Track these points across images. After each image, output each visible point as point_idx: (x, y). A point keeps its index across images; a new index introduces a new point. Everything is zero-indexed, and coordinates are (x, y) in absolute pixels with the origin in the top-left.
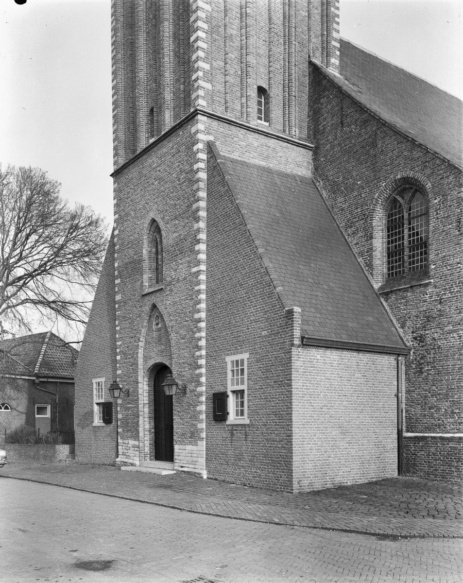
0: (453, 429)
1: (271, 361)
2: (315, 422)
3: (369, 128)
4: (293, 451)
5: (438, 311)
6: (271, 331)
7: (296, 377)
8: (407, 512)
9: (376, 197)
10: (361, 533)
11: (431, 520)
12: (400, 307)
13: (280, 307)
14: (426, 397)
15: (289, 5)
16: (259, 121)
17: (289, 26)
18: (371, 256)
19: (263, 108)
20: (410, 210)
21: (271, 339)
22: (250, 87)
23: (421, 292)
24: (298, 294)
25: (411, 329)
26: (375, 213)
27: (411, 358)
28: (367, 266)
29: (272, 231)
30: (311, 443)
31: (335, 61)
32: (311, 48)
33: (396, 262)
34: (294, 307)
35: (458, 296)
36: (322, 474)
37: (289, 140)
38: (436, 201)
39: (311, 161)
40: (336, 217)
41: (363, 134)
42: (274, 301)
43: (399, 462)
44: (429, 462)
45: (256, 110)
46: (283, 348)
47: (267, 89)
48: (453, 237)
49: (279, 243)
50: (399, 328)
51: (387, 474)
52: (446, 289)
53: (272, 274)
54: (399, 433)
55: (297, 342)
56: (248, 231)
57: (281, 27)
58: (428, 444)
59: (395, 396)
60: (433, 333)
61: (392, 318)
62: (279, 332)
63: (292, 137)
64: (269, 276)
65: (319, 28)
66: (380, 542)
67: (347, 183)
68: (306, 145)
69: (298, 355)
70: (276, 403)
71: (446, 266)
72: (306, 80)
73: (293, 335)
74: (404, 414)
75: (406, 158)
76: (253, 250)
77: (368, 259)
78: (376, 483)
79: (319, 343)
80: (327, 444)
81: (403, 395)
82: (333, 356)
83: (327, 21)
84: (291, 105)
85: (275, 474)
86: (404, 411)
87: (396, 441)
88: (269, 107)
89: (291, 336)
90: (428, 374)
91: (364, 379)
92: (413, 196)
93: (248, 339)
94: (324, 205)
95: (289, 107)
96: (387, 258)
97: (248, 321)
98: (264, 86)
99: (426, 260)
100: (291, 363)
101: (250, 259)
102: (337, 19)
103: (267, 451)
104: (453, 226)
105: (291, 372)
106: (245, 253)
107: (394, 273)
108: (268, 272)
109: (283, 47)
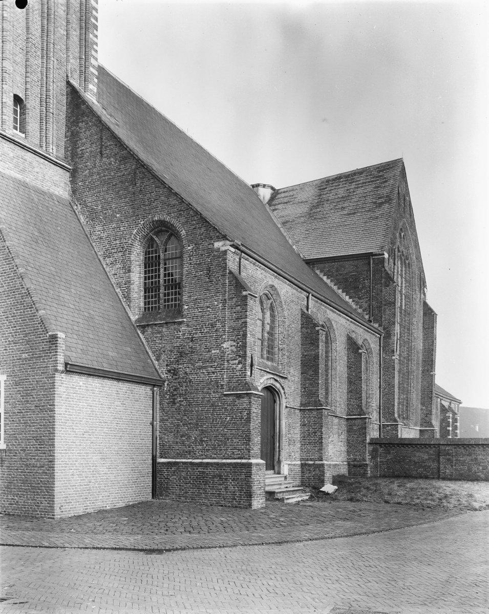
0: (202, 455)
1: (32, 384)
2: (76, 448)
3: (128, 165)
4: (56, 477)
5: (189, 348)
6: (33, 355)
7: (59, 402)
8: (167, 530)
9: (134, 233)
10: (130, 549)
11: (188, 535)
12: (155, 341)
13: (43, 331)
14: (178, 425)
15: (48, 20)
16: (15, 131)
17: (47, 40)
18: (128, 288)
19: (18, 117)
20: (166, 251)
21: (32, 362)
22: (6, 93)
23: (175, 329)
24: (59, 319)
25: (166, 363)
26: (133, 248)
27: (165, 389)
28: (125, 298)
29: (31, 250)
30: (73, 468)
31: (92, 87)
32: (69, 68)
33: (152, 298)
34: (58, 333)
35: (207, 336)
36: (83, 499)
37: (47, 157)
38: (189, 248)
39: (69, 183)
40: (94, 244)
41: (122, 169)
42: (36, 324)
43: (153, 486)
44: (180, 485)
45: (12, 119)
46: (46, 373)
47: (24, 100)
48: (204, 283)
49: (38, 264)
50: (155, 360)
51: (143, 498)
52: (197, 329)
53: (34, 297)
54: (154, 459)
55: (61, 367)
56: (7, 247)
57: (39, 39)
58: (180, 469)
59: (151, 424)
60: (185, 368)
61: (148, 350)
62: (42, 356)
63: (50, 155)
64: (31, 298)
65: (77, 50)
66: (149, 556)
67: (106, 213)
68: (63, 166)
69: (61, 380)
70: (37, 428)
71: (197, 308)
72: (64, 100)
73: (57, 360)
74: (158, 441)
75: (163, 203)
76: (13, 268)
77: (126, 291)
78: (133, 506)
79: (82, 370)
80: (88, 469)
81: (157, 424)
82: (95, 383)
83: (85, 46)
84: (49, 121)
85: (36, 500)
86: (158, 439)
87: (151, 466)
88: (25, 119)
89: (54, 361)
90: (181, 405)
91: (123, 406)
92: (169, 238)
93: (5, 361)
94: (82, 229)
95: (46, 123)
96: (143, 292)
97: (6, 342)
98: (20, 96)
99: (181, 300)
100: (54, 388)
101: (8, 277)
102: (95, 47)
103: (26, 478)
104: (203, 273)
105: (54, 397)
106: (3, 271)
107: (150, 308)
108: (29, 293)
109: (40, 59)
